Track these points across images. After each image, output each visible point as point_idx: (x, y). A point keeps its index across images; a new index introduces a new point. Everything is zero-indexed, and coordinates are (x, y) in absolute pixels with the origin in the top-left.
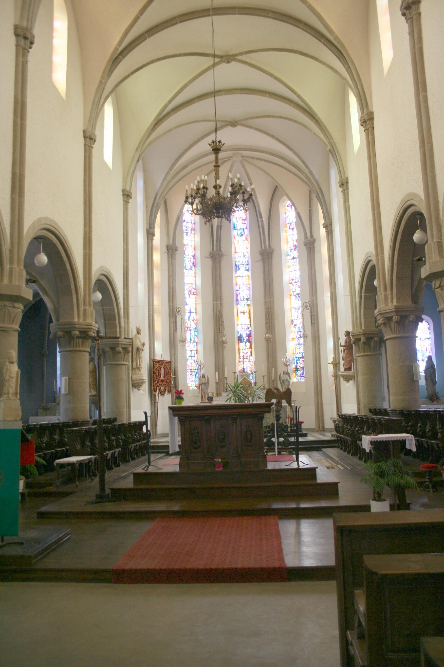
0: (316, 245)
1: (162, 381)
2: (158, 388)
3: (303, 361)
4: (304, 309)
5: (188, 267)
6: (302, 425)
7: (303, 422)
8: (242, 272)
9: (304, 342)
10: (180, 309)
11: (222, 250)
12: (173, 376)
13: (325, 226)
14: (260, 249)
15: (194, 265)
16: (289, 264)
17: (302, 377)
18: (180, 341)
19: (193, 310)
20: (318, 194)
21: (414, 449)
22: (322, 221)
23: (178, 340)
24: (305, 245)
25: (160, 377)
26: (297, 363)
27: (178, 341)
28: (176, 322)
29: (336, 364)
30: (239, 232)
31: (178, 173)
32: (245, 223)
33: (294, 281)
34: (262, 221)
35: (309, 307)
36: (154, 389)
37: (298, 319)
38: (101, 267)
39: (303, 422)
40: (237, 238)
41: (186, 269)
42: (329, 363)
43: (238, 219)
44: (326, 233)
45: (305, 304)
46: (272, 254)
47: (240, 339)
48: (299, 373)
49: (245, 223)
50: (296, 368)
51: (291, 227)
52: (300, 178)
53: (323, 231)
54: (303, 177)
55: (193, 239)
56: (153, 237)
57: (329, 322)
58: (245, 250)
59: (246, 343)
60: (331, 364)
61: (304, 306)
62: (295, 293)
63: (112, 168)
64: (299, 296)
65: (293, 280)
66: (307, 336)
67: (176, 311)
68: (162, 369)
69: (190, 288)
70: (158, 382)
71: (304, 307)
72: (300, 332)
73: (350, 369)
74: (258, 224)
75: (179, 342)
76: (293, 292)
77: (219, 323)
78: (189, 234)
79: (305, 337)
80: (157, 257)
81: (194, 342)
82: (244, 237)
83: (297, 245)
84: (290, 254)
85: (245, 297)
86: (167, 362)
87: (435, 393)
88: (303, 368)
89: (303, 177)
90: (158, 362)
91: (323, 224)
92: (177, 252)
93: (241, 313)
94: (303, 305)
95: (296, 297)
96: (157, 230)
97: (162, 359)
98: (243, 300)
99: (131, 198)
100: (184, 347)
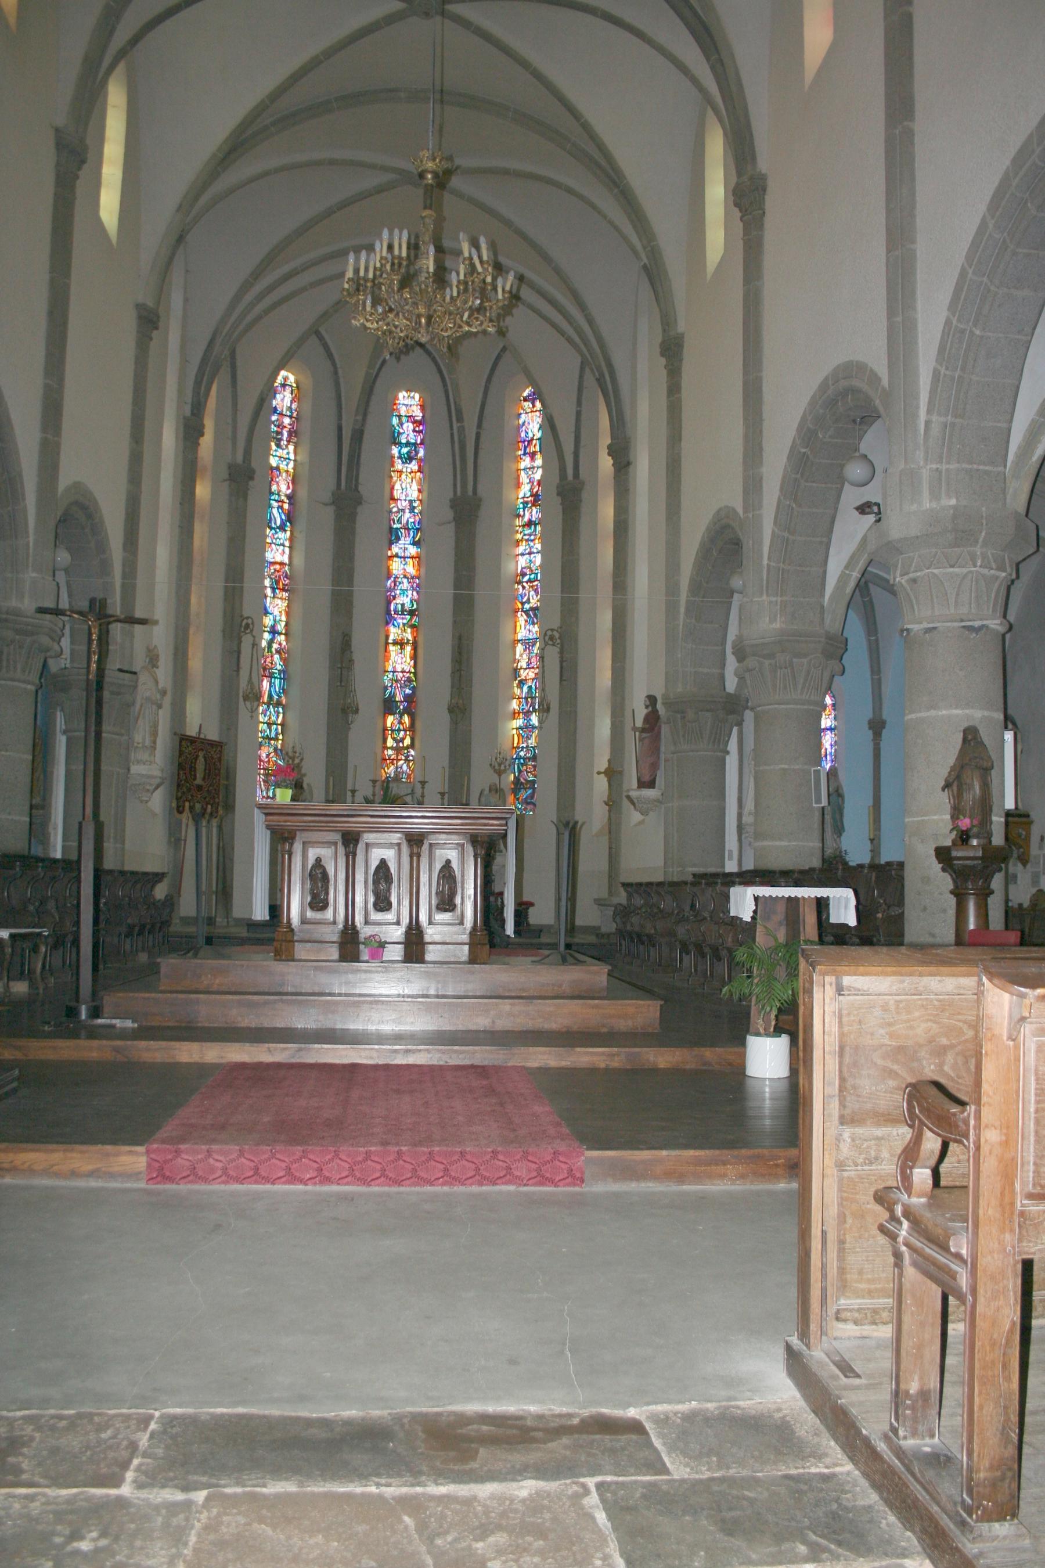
0: (585, 495)
1: (199, 788)
2: (187, 804)
3: (534, 766)
4: (546, 644)
5: (277, 516)
6: (531, 910)
7: (532, 904)
8: (405, 546)
9: (540, 722)
10: (250, 621)
11: (360, 489)
12: (223, 782)
13: (612, 451)
14: (451, 495)
15: (290, 517)
16: (519, 536)
17: (528, 803)
18: (246, 698)
19: (281, 627)
20: (602, 375)
21: (852, 922)
22: (605, 440)
23: (241, 694)
24: (558, 494)
25: (195, 779)
26: (520, 771)
27: (241, 699)
28: (239, 652)
29: (613, 773)
30: (405, 450)
31: (271, 289)
32: (420, 432)
33: (526, 578)
34: (462, 430)
35: (558, 641)
36: (178, 807)
37: (529, 667)
38: (77, 485)
39: (532, 904)
40: (399, 465)
41: (271, 528)
42: (599, 773)
43: (404, 419)
44: (612, 468)
45: (549, 633)
46: (479, 506)
47: (389, 706)
48: (524, 794)
49: (420, 432)
50: (517, 780)
51: (528, 450)
52: (562, 333)
53: (606, 463)
54: (571, 332)
55: (292, 456)
56: (198, 439)
57: (604, 678)
58: (414, 494)
59: (401, 717)
60: (603, 776)
61: (547, 638)
62: (527, 606)
63: (118, 242)
64: (535, 615)
65: (523, 574)
66: (548, 710)
67: (241, 626)
68: (201, 759)
69: (277, 574)
70: (189, 790)
71: (547, 638)
72: (532, 698)
73: (651, 784)
74: (452, 435)
75: (245, 700)
76: (523, 604)
77: (342, 662)
78: (284, 443)
79: (544, 709)
80: (203, 491)
81: (278, 704)
82: (414, 466)
83: (540, 493)
84: (522, 513)
85: (408, 606)
86: (212, 744)
87: (841, 852)
88: (534, 782)
89: (571, 332)
90: (192, 740)
91: (609, 447)
92: (251, 483)
93: (395, 643)
94: (545, 634)
95: (528, 615)
96: (209, 424)
97: (202, 736)
98: (403, 614)
99: (157, 328)
100: (254, 711)
